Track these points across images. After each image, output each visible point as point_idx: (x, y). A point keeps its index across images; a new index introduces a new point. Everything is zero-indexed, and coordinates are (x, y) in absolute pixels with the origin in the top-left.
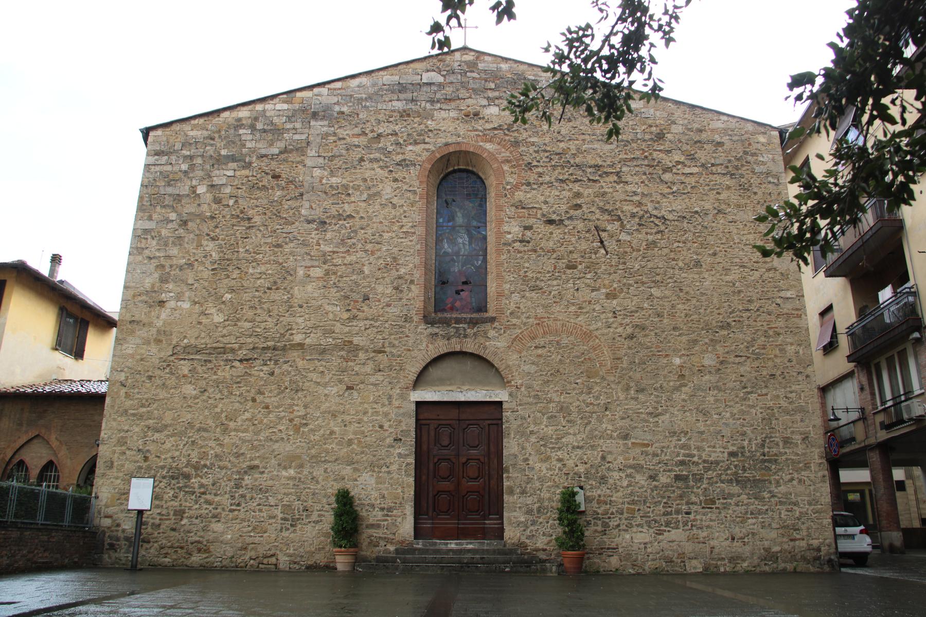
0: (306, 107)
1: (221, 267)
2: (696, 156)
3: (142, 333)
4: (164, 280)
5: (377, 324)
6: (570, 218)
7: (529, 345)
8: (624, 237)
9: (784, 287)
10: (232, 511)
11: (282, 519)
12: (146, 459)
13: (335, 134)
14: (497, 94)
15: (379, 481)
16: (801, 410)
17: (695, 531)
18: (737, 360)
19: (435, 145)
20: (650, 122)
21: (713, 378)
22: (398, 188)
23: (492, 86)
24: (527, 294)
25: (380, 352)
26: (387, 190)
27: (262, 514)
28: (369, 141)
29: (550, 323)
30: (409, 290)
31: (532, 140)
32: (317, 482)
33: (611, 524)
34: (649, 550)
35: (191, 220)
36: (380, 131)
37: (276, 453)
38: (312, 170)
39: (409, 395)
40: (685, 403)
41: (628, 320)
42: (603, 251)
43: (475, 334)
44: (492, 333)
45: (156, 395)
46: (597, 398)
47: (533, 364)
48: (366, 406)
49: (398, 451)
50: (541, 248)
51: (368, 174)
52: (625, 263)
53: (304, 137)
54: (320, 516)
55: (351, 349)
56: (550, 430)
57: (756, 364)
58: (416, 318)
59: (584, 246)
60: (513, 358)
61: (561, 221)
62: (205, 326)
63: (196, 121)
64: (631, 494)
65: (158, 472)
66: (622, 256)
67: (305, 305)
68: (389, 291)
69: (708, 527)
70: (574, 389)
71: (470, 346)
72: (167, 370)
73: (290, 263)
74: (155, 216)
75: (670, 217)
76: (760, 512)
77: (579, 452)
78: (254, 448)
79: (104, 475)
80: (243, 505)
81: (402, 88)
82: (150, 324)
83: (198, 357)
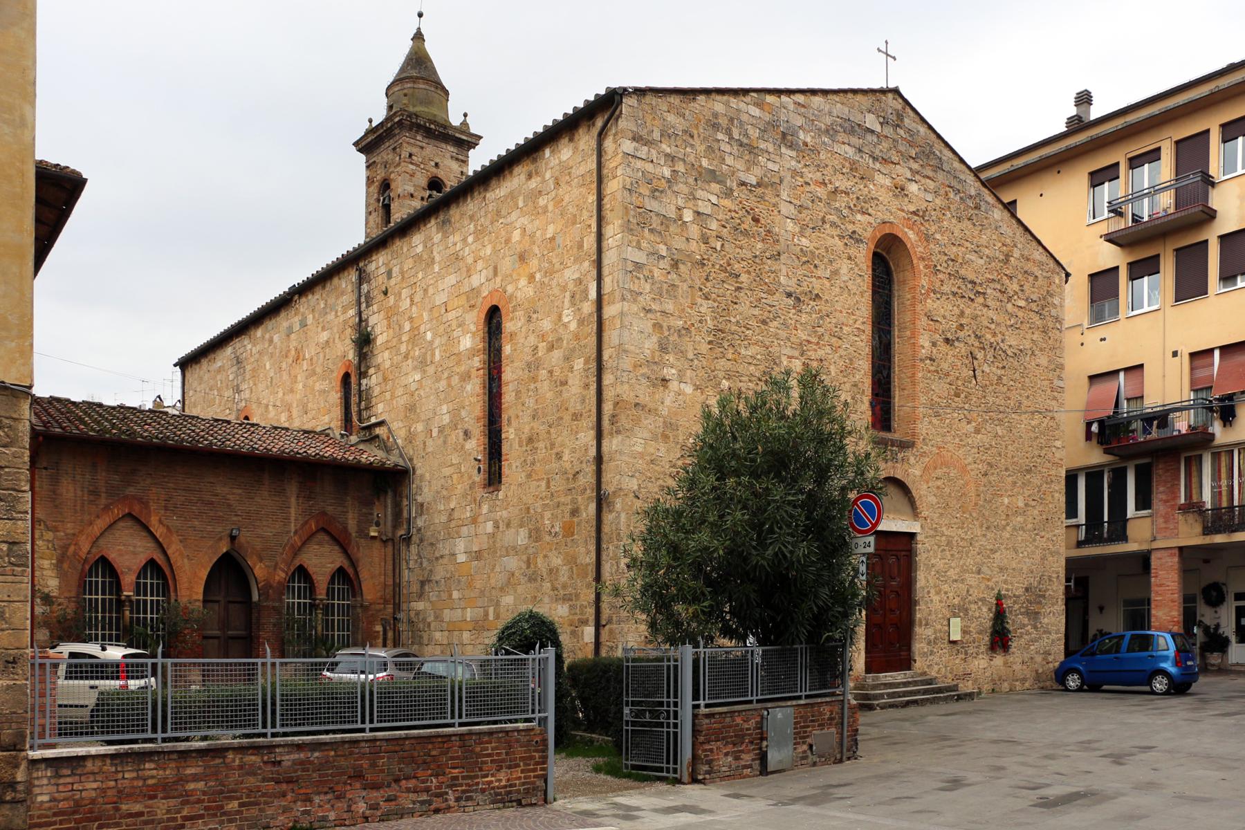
0: (35, 23)
44: (912, 460)
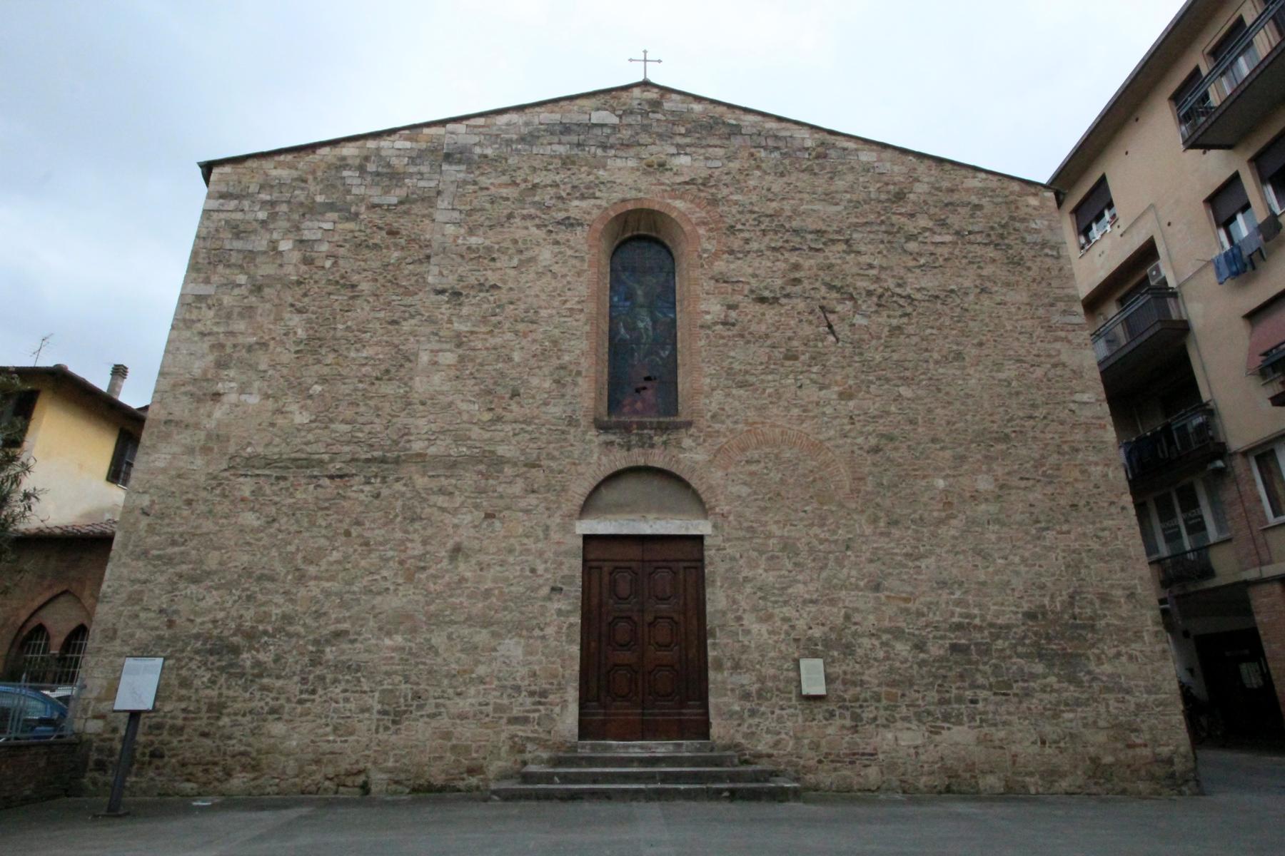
0: (440, 147)
1: (312, 346)
2: (948, 221)
3: (185, 438)
4: (221, 365)
5: (530, 428)
6: (788, 296)
7: (738, 458)
8: (859, 320)
9: (1078, 389)
10: (301, 702)
11: (379, 712)
12: (171, 624)
13: (475, 183)
14: (688, 140)
15: (529, 652)
16: (1121, 555)
17: (986, 729)
18: (1023, 484)
19: (608, 201)
20: (885, 179)
21: (993, 508)
22: (560, 253)
23: (683, 130)
24: (734, 391)
25: (534, 466)
26: (546, 255)
27: (348, 706)
28: (521, 193)
29: (766, 429)
30: (575, 384)
31: (735, 197)
32: (437, 654)
33: (865, 715)
34: (923, 758)
35: (268, 286)
36: (536, 181)
37: (377, 611)
38: (443, 225)
39: (573, 525)
40: (905, 554)
41: (870, 428)
42: (831, 338)
43: (665, 443)
44: (687, 442)
45: (197, 527)
46: (834, 532)
47: (745, 483)
48: (512, 540)
49: (556, 606)
50: (750, 333)
51: (520, 234)
52: (861, 354)
53: (433, 184)
54: (437, 706)
55: (497, 463)
56: (770, 578)
57: (1049, 490)
58: (583, 422)
59: (807, 330)
60: (717, 476)
61: (776, 300)
62: (281, 429)
63: (282, 158)
64: (891, 670)
65: (187, 644)
66: (857, 345)
67: (429, 402)
68: (547, 384)
69: (1004, 723)
70: (801, 520)
71: (657, 459)
72: (218, 491)
73: (411, 345)
74: (215, 278)
75: (918, 296)
76: (1078, 703)
77: (813, 608)
78: (343, 605)
79: (99, 650)
80: (320, 692)
81: (566, 129)
82: (197, 426)
83: (267, 472)
